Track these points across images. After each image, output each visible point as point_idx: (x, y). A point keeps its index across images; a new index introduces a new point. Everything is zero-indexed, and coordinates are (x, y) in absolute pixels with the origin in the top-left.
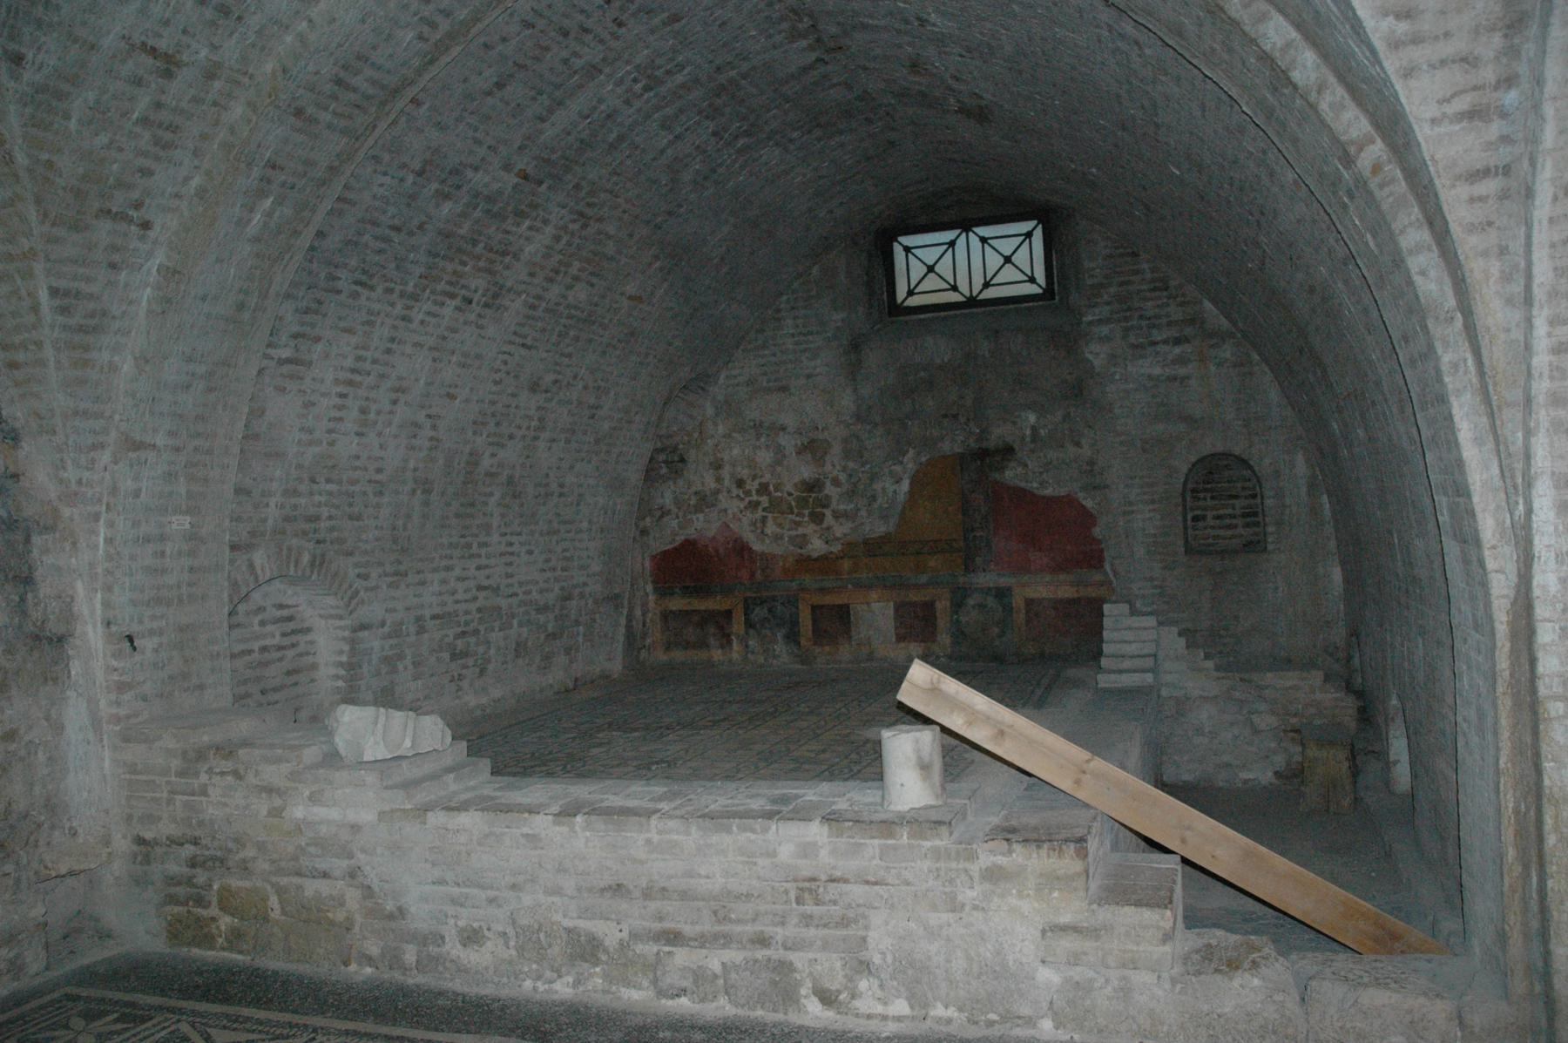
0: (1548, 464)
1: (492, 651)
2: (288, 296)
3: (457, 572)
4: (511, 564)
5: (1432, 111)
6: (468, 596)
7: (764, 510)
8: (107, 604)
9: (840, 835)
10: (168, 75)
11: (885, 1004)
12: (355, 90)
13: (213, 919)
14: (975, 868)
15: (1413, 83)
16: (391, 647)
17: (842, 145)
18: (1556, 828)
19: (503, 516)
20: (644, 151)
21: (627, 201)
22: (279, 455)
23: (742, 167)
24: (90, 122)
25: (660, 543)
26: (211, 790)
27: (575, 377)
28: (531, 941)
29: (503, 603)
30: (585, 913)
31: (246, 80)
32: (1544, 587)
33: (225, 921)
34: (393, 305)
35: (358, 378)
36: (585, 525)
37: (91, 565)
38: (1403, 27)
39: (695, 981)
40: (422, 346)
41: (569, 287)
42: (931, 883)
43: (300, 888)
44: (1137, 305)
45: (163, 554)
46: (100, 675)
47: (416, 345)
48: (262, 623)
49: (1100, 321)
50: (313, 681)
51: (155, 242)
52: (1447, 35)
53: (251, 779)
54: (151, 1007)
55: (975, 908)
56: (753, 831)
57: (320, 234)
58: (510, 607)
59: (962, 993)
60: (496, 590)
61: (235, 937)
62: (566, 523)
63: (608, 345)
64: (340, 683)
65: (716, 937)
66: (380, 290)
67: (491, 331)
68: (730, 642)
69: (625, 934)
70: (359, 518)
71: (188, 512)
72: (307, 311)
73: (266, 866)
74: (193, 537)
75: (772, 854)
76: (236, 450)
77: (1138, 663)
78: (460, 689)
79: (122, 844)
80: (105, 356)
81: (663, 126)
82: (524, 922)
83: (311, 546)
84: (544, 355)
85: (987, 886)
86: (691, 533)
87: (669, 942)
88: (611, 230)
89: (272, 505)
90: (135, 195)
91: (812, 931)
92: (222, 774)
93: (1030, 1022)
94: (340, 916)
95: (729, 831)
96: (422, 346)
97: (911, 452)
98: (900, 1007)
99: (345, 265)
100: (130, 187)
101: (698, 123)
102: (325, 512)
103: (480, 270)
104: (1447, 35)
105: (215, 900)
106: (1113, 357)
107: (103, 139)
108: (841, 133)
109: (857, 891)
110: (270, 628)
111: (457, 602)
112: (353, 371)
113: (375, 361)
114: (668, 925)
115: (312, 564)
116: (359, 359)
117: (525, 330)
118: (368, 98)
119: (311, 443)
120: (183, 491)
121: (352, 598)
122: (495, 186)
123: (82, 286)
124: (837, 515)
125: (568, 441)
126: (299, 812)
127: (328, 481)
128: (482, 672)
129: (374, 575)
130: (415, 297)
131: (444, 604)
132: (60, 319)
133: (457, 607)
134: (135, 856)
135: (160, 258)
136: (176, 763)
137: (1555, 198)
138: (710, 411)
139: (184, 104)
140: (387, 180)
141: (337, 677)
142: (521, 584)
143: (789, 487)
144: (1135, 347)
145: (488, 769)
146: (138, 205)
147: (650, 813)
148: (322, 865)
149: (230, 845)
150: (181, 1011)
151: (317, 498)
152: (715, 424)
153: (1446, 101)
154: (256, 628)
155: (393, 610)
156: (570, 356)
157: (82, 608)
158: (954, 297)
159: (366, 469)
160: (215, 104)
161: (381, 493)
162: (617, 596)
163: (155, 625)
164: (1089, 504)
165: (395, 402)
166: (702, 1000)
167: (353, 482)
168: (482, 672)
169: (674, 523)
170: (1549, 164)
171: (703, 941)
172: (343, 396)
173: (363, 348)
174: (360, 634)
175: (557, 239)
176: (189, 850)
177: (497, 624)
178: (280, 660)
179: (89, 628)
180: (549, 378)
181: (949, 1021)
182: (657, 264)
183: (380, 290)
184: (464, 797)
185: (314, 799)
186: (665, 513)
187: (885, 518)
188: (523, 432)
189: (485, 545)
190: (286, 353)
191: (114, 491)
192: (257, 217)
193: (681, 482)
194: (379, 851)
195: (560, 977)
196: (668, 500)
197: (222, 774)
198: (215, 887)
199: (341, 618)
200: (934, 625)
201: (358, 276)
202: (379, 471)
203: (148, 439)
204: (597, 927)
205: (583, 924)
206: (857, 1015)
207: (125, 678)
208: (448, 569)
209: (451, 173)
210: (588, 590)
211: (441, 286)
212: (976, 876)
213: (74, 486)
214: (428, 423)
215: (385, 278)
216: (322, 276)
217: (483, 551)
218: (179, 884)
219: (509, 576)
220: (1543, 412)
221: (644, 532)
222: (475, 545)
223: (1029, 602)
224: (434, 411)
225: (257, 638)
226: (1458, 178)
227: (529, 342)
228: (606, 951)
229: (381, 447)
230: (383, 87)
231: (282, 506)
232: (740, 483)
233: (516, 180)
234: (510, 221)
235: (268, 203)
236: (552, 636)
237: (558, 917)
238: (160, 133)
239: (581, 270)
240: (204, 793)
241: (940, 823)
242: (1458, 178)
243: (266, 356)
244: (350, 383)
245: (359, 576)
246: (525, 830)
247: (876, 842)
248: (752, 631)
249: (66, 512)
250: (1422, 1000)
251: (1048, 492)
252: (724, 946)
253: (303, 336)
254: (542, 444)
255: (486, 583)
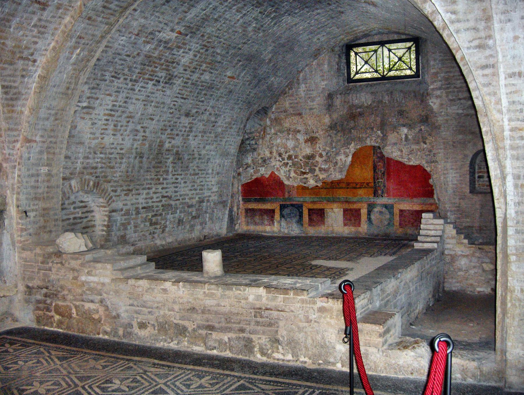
0: (511, 170)
1: (168, 223)
2: (86, 83)
3: (154, 190)
4: (177, 187)
5: (466, 45)
6: (158, 200)
7: (290, 166)
8: (18, 199)
9: (270, 292)
10: (44, 9)
11: (284, 355)
12: (110, 9)
13: (53, 317)
14: (316, 307)
15: (459, 35)
16: (125, 220)
17: (318, 14)
18: (511, 301)
19: (173, 167)
20: (230, 21)
21: (225, 40)
22: (82, 143)
23: (275, 24)
24: (17, 28)
25: (245, 179)
26: (53, 269)
27: (206, 110)
28: (163, 327)
29: (173, 203)
30: (182, 318)
31: (71, 8)
32: (510, 214)
33: (57, 317)
34: (127, 84)
35: (113, 113)
36: (210, 171)
37: (13, 185)
38: (453, 17)
39: (219, 344)
40: (139, 100)
41: (202, 74)
42: (300, 312)
43: (83, 306)
44: (454, 82)
45: (38, 181)
46: (15, 225)
47: (137, 99)
48: (75, 208)
49: (437, 89)
50: (93, 231)
51: (38, 67)
52: (468, 20)
53: (67, 265)
54: (31, 343)
55: (315, 322)
56: (240, 290)
57: (98, 60)
58: (176, 204)
59: (310, 353)
60: (170, 198)
61: (60, 324)
62: (201, 170)
63: (220, 97)
64: (104, 233)
65: (226, 328)
66: (122, 79)
67: (168, 92)
68: (273, 223)
69: (195, 326)
70: (113, 168)
71: (48, 165)
72: (93, 88)
73: (72, 297)
74: (49, 174)
75: (246, 299)
76: (65, 142)
77: (433, 239)
78: (154, 237)
79: (21, 288)
80: (19, 108)
81: (237, 11)
82: (161, 320)
83: (94, 178)
84: (192, 102)
85: (320, 314)
86: (258, 175)
87: (210, 330)
88: (219, 51)
89: (79, 162)
90: (31, 51)
91: (259, 328)
92: (57, 263)
93: (334, 364)
94: (96, 317)
95: (232, 290)
96: (139, 100)
97: (352, 145)
98: (289, 357)
99: (108, 71)
100: (29, 49)
101: (253, 9)
102: (100, 165)
103: (163, 69)
104: (468, 20)
105: (53, 309)
106: (442, 105)
107: (21, 33)
108: (317, 9)
109: (275, 314)
110: (77, 210)
111: (153, 202)
112: (111, 110)
113: (120, 106)
114: (210, 323)
115: (94, 185)
116: (114, 105)
117: (184, 92)
118: (115, 11)
119: (94, 139)
120: (46, 158)
121: (109, 199)
122: (168, 37)
123: (13, 84)
124: (321, 170)
125: (202, 136)
126: (83, 278)
127: (101, 153)
128: (163, 231)
129: (119, 191)
130: (136, 81)
131: (147, 203)
132: (5, 96)
133: (153, 204)
134: (26, 292)
135: (39, 72)
136: (40, 259)
137: (506, 78)
138: (268, 123)
139: (49, 19)
140: (124, 38)
141: (103, 230)
142: (181, 196)
143: (300, 158)
144: (451, 100)
145: (154, 267)
146: (32, 54)
147: (205, 283)
148: (91, 298)
149: (59, 289)
150: (41, 345)
151: (97, 160)
152: (270, 128)
153: (470, 42)
154: (72, 210)
155: (126, 205)
156: (203, 101)
157: (9, 200)
158: (376, 75)
159: (116, 148)
160: (60, 17)
161: (123, 158)
162: (224, 201)
163: (34, 208)
164: (428, 169)
165: (128, 122)
166: (221, 352)
167: (111, 154)
168: (163, 231)
169: (252, 171)
170: (502, 67)
171: (223, 330)
172: (107, 120)
173: (115, 101)
174: (113, 214)
175: (195, 56)
176: (45, 290)
177: (170, 212)
178: (81, 223)
179: (12, 208)
180: (194, 111)
181: (305, 362)
182: (241, 63)
183: (122, 79)
184: (142, 275)
185: (89, 273)
186: (248, 166)
187: (341, 172)
188: (182, 133)
189: (166, 179)
190: (85, 104)
191: (21, 157)
192: (74, 56)
193: (255, 153)
194: (111, 293)
195: (172, 341)
196: (249, 161)
197: (57, 263)
198: (54, 305)
199: (105, 207)
200: (360, 219)
201: (113, 74)
202: (121, 149)
203: (34, 138)
204: (186, 323)
205: (181, 322)
206: (274, 359)
207: (24, 227)
208: (149, 188)
209: (149, 34)
210: (211, 199)
211: (147, 76)
212: (316, 310)
213: (7, 156)
214: (142, 130)
215: (124, 74)
216: (99, 75)
217: (165, 182)
218: (40, 303)
219: (176, 192)
220: (508, 152)
221: (239, 174)
222: (161, 179)
223: (401, 211)
224: (145, 125)
225: (72, 214)
226: (478, 68)
227: (185, 97)
228: (189, 332)
229: (122, 140)
230: (121, 7)
231: (83, 163)
232: (280, 155)
233: (177, 35)
234: (175, 50)
235: (78, 51)
236: (194, 218)
237: (172, 319)
238: (40, 29)
239: (207, 67)
240: (50, 270)
241: (304, 290)
242: (478, 68)
243: (78, 106)
244: (110, 115)
245: (112, 191)
246: (162, 287)
247: (282, 296)
248: (283, 219)
249: (4, 165)
250: (467, 362)
251: (411, 163)
252: (229, 332)
253: (92, 98)
254: (190, 138)
255: (166, 195)
